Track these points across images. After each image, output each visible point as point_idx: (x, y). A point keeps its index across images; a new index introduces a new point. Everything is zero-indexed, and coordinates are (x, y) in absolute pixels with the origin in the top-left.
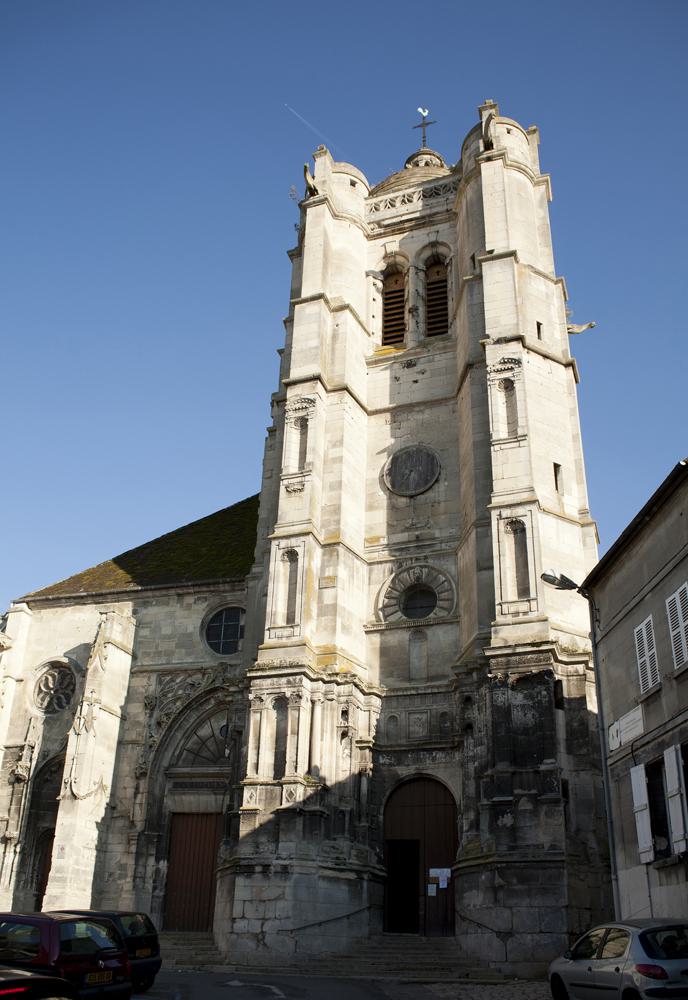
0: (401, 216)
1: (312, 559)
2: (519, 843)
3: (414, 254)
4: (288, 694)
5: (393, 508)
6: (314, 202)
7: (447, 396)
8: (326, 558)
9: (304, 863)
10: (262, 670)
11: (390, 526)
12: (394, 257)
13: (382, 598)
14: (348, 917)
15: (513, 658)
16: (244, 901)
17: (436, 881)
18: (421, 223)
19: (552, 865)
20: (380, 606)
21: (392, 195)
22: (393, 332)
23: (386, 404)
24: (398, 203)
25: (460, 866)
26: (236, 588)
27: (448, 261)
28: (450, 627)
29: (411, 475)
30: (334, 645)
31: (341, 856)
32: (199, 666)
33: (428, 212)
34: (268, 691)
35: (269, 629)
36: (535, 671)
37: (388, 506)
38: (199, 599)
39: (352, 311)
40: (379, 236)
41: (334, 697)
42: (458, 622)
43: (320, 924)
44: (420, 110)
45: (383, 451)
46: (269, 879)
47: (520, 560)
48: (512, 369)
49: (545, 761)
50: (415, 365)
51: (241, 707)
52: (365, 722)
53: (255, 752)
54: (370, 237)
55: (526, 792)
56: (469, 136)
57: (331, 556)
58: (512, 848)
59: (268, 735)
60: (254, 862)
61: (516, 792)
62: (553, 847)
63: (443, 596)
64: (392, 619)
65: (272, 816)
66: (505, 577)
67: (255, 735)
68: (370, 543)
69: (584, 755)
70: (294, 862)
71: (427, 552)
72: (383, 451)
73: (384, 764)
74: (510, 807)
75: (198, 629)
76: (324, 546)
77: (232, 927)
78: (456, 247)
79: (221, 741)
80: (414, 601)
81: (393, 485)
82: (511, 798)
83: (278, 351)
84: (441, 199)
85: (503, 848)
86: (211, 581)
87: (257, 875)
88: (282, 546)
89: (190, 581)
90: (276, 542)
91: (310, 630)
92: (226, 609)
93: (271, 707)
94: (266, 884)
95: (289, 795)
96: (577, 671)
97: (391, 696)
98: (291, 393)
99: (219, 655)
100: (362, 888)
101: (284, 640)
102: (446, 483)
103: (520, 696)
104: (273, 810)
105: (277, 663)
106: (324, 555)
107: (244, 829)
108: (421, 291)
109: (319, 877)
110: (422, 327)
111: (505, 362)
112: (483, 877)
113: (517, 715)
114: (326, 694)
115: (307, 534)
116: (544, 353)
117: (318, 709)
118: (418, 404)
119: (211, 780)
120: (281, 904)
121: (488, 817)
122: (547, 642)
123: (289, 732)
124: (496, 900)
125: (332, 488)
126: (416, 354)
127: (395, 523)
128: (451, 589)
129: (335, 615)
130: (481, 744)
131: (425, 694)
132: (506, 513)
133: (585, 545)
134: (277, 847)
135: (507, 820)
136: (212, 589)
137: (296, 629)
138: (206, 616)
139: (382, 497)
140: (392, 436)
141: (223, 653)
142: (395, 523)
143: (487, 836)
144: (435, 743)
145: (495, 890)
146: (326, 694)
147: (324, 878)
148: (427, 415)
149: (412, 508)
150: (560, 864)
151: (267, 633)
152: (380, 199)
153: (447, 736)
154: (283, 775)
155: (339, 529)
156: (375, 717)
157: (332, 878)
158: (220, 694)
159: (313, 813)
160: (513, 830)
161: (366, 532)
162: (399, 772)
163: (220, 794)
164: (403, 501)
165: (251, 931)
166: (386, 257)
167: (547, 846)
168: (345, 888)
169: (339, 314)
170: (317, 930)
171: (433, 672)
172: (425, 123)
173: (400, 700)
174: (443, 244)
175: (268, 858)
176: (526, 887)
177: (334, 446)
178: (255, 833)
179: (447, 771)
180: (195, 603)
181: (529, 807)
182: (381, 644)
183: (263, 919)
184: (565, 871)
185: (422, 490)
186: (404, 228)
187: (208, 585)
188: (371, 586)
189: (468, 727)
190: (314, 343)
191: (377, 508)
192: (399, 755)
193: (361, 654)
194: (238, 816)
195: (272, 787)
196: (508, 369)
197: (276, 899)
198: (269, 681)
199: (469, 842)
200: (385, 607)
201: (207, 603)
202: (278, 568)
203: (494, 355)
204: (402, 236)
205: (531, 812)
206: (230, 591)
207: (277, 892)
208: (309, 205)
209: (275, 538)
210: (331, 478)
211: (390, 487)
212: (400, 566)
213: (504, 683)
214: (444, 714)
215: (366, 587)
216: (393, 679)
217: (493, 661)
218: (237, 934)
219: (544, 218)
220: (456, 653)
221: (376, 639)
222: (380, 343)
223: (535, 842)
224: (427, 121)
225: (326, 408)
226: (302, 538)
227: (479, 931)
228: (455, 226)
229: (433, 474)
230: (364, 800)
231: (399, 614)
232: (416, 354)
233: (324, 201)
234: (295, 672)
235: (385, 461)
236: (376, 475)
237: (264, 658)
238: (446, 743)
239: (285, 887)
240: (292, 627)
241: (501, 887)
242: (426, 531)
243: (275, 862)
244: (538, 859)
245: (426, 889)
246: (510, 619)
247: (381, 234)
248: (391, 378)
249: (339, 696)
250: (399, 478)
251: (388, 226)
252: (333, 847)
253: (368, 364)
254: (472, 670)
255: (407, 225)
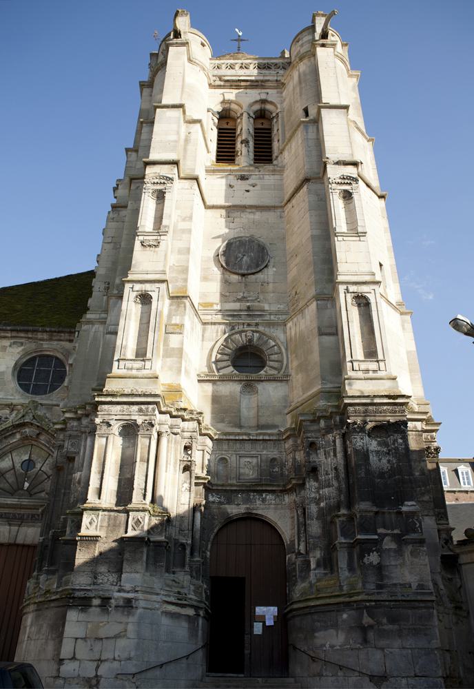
0: (240, 76)
1: (162, 305)
2: (386, 581)
3: (248, 104)
4: (139, 422)
5: (225, 282)
6: (177, 43)
7: (276, 204)
8: (173, 308)
9: (149, 596)
10: (113, 395)
11: (222, 295)
12: (230, 103)
13: (214, 353)
14: (187, 657)
15: (370, 408)
16: (77, 639)
17: (262, 619)
18: (254, 85)
19: (422, 605)
20: (213, 359)
21: (232, 61)
22: (226, 153)
23: (221, 201)
24: (237, 67)
25: (295, 606)
26: (54, 338)
27: (274, 114)
28: (279, 384)
29: (243, 259)
30: (179, 384)
31: (182, 591)
32: (9, 402)
33: (261, 78)
34: (118, 417)
35: (118, 360)
36: (392, 420)
37: (221, 281)
38: (14, 343)
39: (202, 126)
40: (219, 87)
41: (179, 431)
42: (287, 381)
43: (161, 666)
44: (237, 30)
45: (218, 237)
46: (108, 612)
47: (365, 329)
48: (350, 184)
49: (406, 503)
50: (247, 179)
51: (75, 433)
52: (202, 457)
53: (99, 476)
54: (211, 86)
55: (389, 532)
56: (301, 32)
57: (178, 306)
58: (380, 587)
59: (113, 461)
60: (91, 594)
61: (380, 531)
62: (421, 586)
63: (273, 357)
64: (222, 372)
65: (114, 545)
66: (354, 339)
67: (99, 459)
68: (204, 307)
69: (425, 502)
70: (140, 595)
71: (258, 320)
72: (218, 237)
73: (213, 502)
74: (375, 545)
75: (11, 370)
76: (172, 298)
77: (58, 670)
78: (286, 102)
79: (21, 474)
80: (245, 359)
81: (227, 263)
82: (376, 537)
83: (126, 149)
84: (273, 72)
85: (371, 587)
86: (31, 328)
87: (93, 609)
88: (135, 289)
89: (9, 326)
90: (131, 285)
91: (158, 365)
92: (40, 356)
93: (117, 433)
94: (105, 618)
95: (136, 523)
96: (415, 427)
97: (222, 440)
98: (150, 171)
99: (28, 395)
100: (198, 624)
101: (134, 372)
102: (275, 269)
103: (374, 443)
104: (115, 538)
105: (127, 391)
106: (171, 305)
107: (81, 557)
108: (252, 131)
109: (162, 612)
110: (252, 155)
111: (344, 178)
112: (345, 616)
113: (373, 459)
114: (171, 427)
115: (163, 281)
116: (368, 182)
117: (164, 440)
118: (251, 207)
119: (6, 511)
120: (122, 643)
121: (346, 554)
122: (403, 396)
123: (138, 460)
124: (365, 641)
125: (180, 252)
126: (249, 171)
127: (228, 294)
128: (281, 353)
129: (181, 358)
130: (329, 486)
131: (256, 440)
132: (352, 288)
133: (404, 329)
134: (120, 579)
135: (373, 558)
136: (30, 336)
137: (147, 363)
138: (20, 358)
139: (217, 273)
140: (226, 227)
141: (33, 393)
142: (228, 294)
143: (347, 573)
144: (267, 485)
145: (364, 630)
146: (171, 427)
147: (167, 613)
148: (258, 216)
149: (243, 285)
150: (429, 604)
151: (115, 364)
152: (222, 61)
153: (273, 481)
154: (130, 500)
155: (186, 286)
156: (207, 457)
157: (175, 614)
158: (27, 430)
159: (158, 544)
160: (380, 568)
161: (200, 298)
162: (229, 511)
163: (15, 525)
164: (235, 278)
165: (83, 675)
166: (223, 102)
167: (414, 586)
168: (185, 624)
169: (192, 125)
170: (158, 672)
171: (263, 421)
172: (239, 40)
173: (231, 443)
174: (271, 103)
175: (108, 590)
176: (396, 627)
177: (184, 220)
178: (95, 562)
179: (278, 513)
180: (10, 346)
181: (393, 546)
182: (213, 392)
183: (100, 660)
184: (435, 611)
185: (254, 271)
186: (241, 86)
187: (27, 331)
188: (204, 342)
189: (314, 471)
190: (174, 137)
191: (211, 280)
192: (229, 494)
193: (197, 397)
194: (74, 543)
195: (116, 514)
196: (347, 183)
197: (116, 637)
198: (119, 407)
199: (319, 580)
200: (217, 361)
201: (23, 347)
202: (130, 309)
203: (334, 173)
204: (237, 91)
205: (395, 551)
206: (47, 340)
207: (116, 629)
208: (172, 45)
209: (129, 281)
210: (180, 244)
211: (224, 265)
212: (233, 328)
213: (362, 429)
214: (273, 460)
215: (200, 342)
216: (223, 424)
217: (351, 409)
218: (64, 678)
219: (356, 98)
220: (285, 407)
221: (209, 388)
222: (215, 160)
223: (401, 582)
224: (241, 38)
225: (178, 192)
226: (157, 285)
227: (340, 673)
228: (282, 93)
229: (263, 261)
230: (197, 536)
231: (231, 369)
232: (249, 171)
233: (186, 44)
234: (148, 401)
235: (220, 245)
236: (212, 254)
237: (110, 386)
238: (278, 486)
239: (127, 623)
240: (143, 360)
241: (371, 627)
242: (256, 304)
243: (116, 595)
244: (408, 599)
245: (252, 627)
246: (360, 374)
247: (221, 86)
248: (226, 185)
249: (183, 431)
250: (233, 259)
251: (228, 81)
252: (174, 581)
253: (207, 171)
254: (319, 418)
255: (243, 84)
